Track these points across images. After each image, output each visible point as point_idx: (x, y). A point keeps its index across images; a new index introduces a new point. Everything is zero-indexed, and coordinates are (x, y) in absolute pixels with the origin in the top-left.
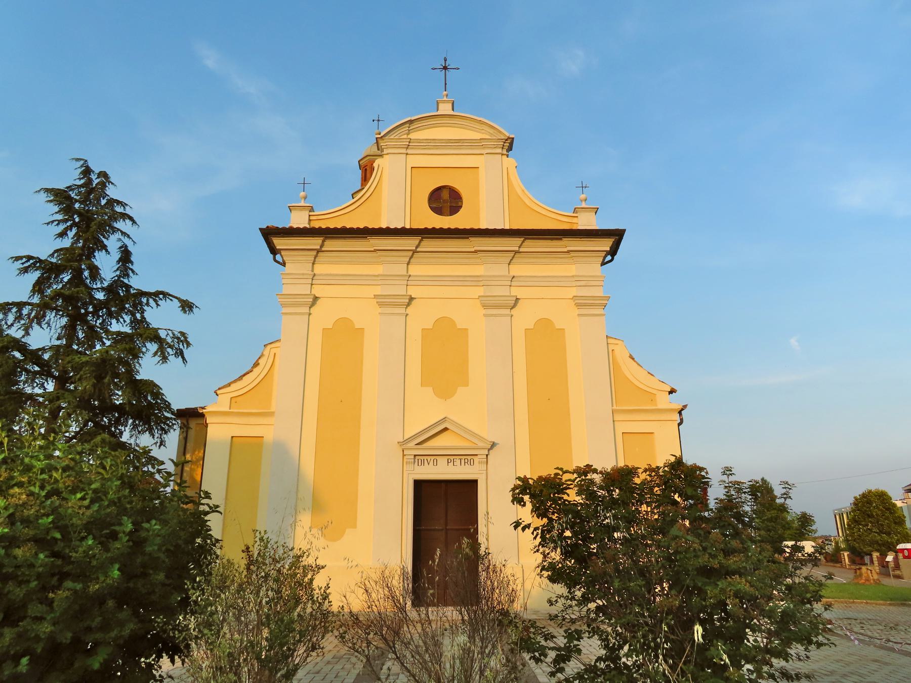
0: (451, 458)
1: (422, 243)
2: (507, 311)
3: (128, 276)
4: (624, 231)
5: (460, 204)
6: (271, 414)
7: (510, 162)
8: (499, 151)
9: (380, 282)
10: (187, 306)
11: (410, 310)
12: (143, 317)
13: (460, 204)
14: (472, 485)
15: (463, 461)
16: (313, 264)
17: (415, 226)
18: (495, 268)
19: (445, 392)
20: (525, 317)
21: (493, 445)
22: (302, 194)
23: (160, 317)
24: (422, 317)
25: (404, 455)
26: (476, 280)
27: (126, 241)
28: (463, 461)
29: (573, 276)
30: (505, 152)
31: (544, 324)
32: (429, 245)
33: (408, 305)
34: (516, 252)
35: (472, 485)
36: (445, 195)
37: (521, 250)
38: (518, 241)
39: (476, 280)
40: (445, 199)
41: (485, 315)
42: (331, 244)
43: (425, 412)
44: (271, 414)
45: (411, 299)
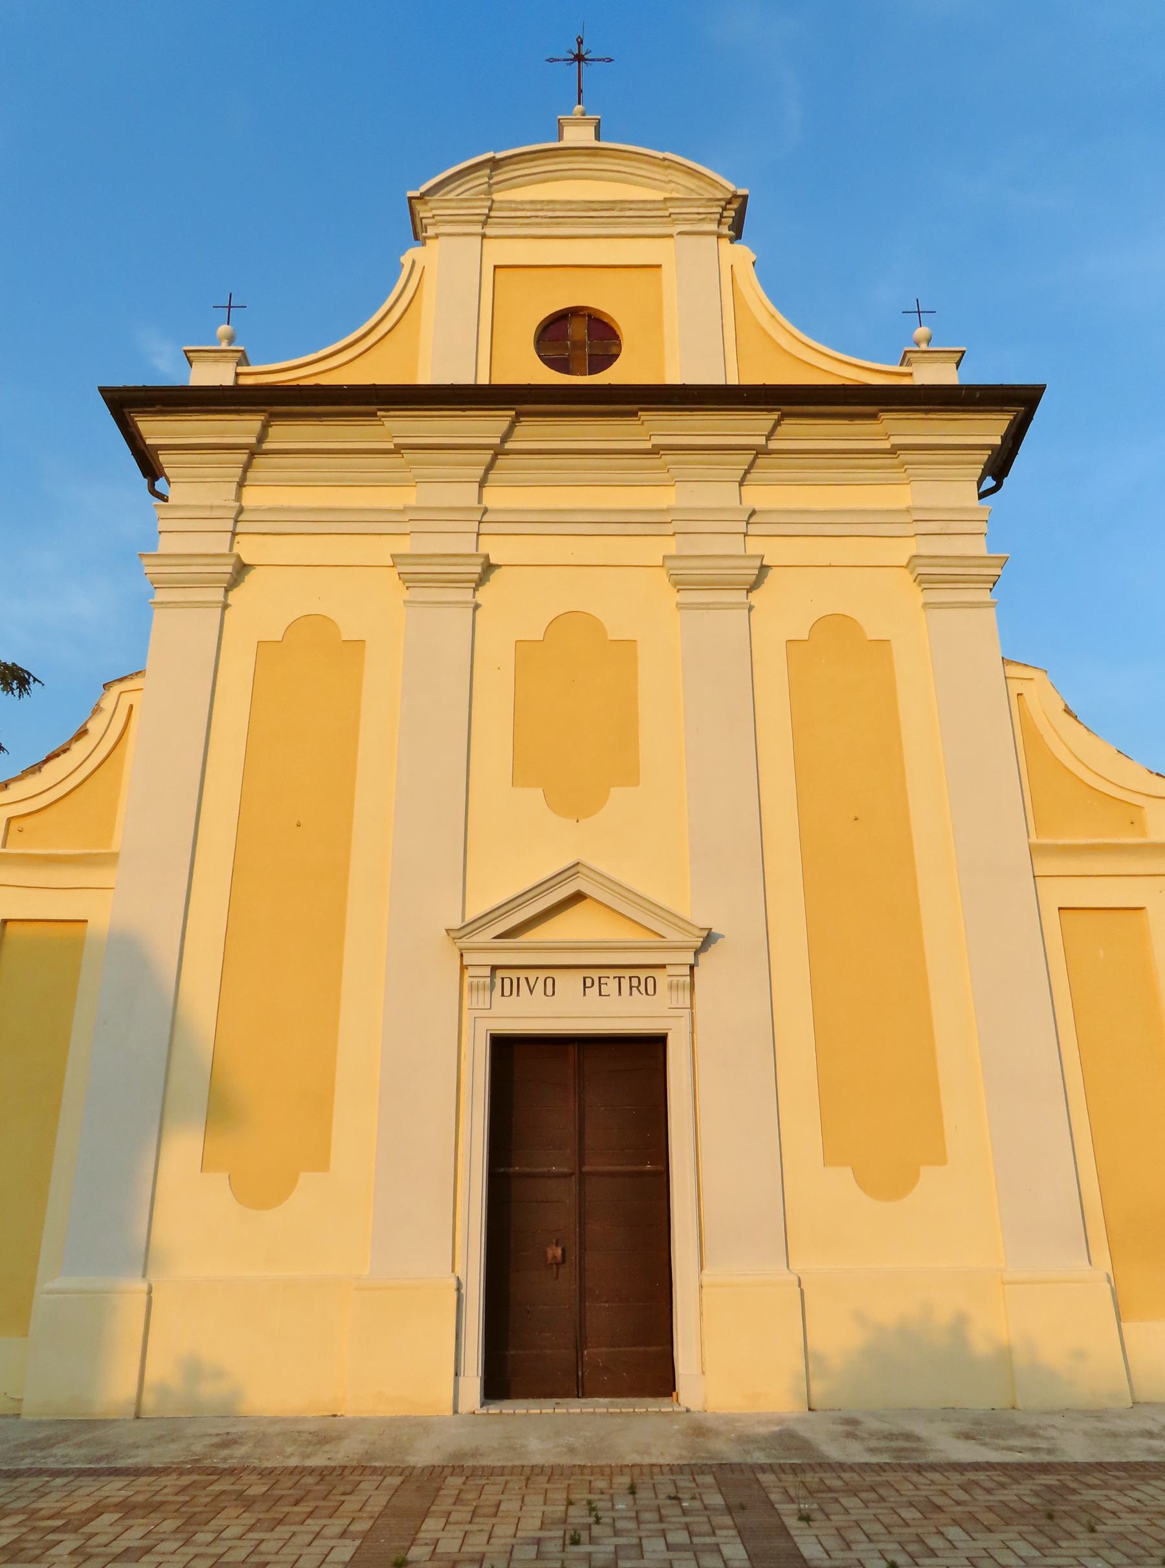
0: (592, 974)
1: (518, 430)
2: (740, 596)
4: (1041, 389)
7: (740, 255)
8: (713, 227)
9: (408, 528)
11: (483, 595)
13: (614, 351)
14: (652, 1047)
15: (625, 984)
16: (241, 485)
17: (500, 379)
18: (711, 492)
19: (575, 800)
20: (785, 611)
21: (709, 939)
22: (224, 329)
24: (516, 610)
25: (463, 968)
26: (654, 522)
28: (625, 984)
29: (908, 510)
30: (725, 230)
31: (836, 629)
32: (536, 433)
33: (481, 581)
34: (761, 451)
35: (652, 1047)
36: (578, 330)
37: (773, 445)
38: (763, 420)
39: (654, 522)
40: (575, 336)
41: (680, 606)
42: (285, 434)
44: (109, 860)
45: (489, 568)
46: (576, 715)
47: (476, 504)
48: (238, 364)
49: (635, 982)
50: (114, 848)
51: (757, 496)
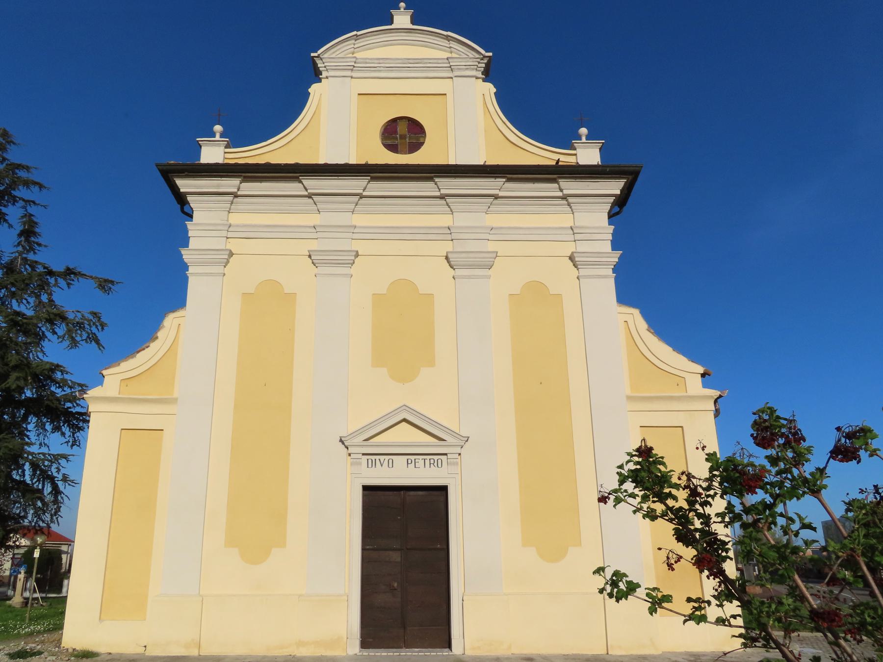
3: (33, 250)
5: (421, 140)
6: (174, 401)
8: (474, 73)
10: (105, 285)
12: (51, 301)
13: (421, 140)
15: (427, 462)
18: (304, 217)
19: (404, 373)
23: (69, 299)
27: (32, 210)
28: (427, 462)
36: (402, 128)
40: (404, 132)
43: (371, 398)
44: (174, 401)
45: (231, 254)
46: (403, 333)
47: (226, 222)
48: (226, 147)
49: (432, 461)
50: (175, 395)
51: (235, 219)
